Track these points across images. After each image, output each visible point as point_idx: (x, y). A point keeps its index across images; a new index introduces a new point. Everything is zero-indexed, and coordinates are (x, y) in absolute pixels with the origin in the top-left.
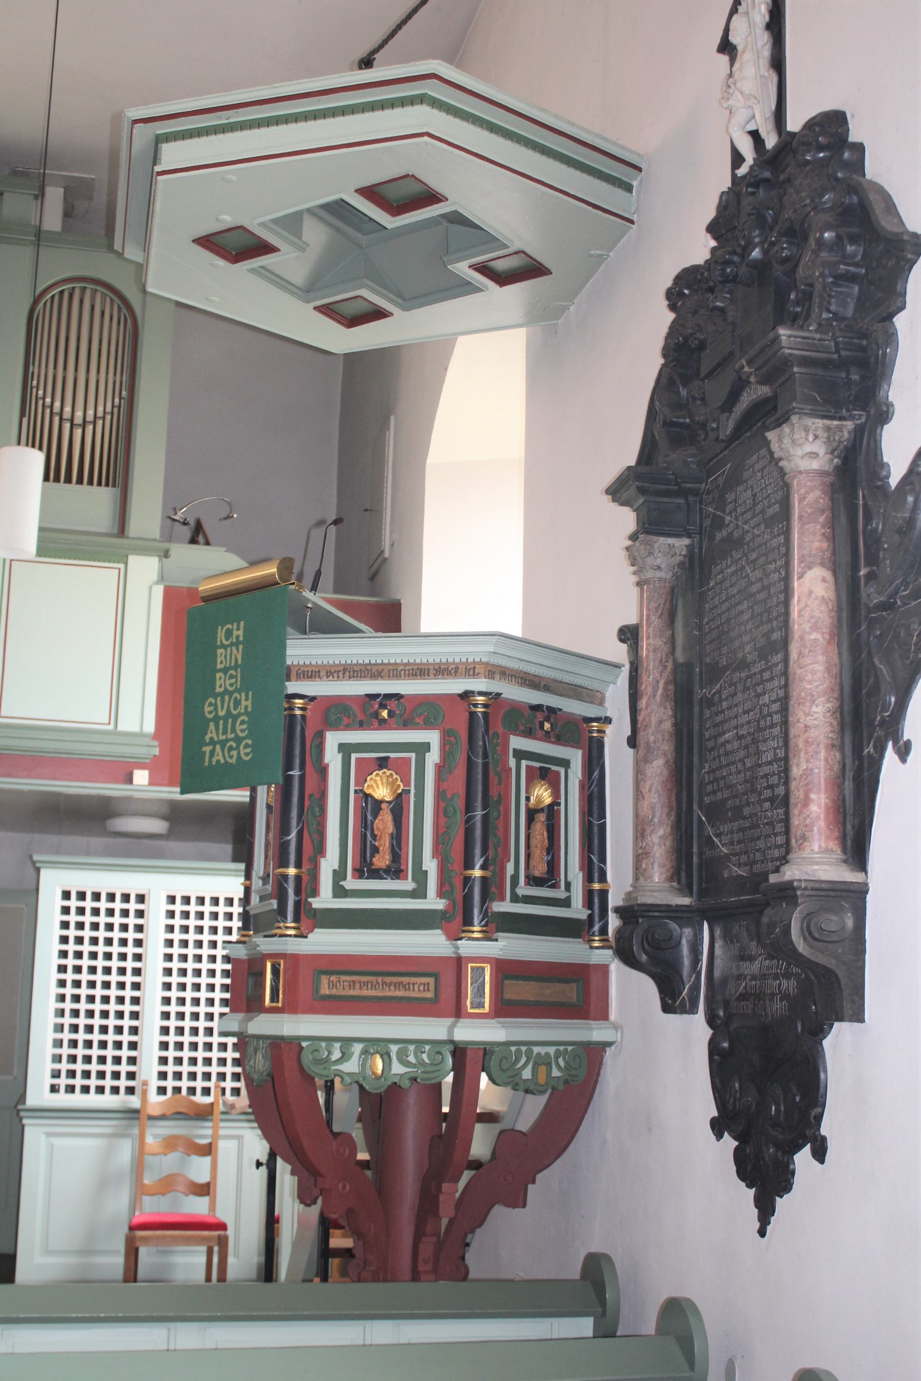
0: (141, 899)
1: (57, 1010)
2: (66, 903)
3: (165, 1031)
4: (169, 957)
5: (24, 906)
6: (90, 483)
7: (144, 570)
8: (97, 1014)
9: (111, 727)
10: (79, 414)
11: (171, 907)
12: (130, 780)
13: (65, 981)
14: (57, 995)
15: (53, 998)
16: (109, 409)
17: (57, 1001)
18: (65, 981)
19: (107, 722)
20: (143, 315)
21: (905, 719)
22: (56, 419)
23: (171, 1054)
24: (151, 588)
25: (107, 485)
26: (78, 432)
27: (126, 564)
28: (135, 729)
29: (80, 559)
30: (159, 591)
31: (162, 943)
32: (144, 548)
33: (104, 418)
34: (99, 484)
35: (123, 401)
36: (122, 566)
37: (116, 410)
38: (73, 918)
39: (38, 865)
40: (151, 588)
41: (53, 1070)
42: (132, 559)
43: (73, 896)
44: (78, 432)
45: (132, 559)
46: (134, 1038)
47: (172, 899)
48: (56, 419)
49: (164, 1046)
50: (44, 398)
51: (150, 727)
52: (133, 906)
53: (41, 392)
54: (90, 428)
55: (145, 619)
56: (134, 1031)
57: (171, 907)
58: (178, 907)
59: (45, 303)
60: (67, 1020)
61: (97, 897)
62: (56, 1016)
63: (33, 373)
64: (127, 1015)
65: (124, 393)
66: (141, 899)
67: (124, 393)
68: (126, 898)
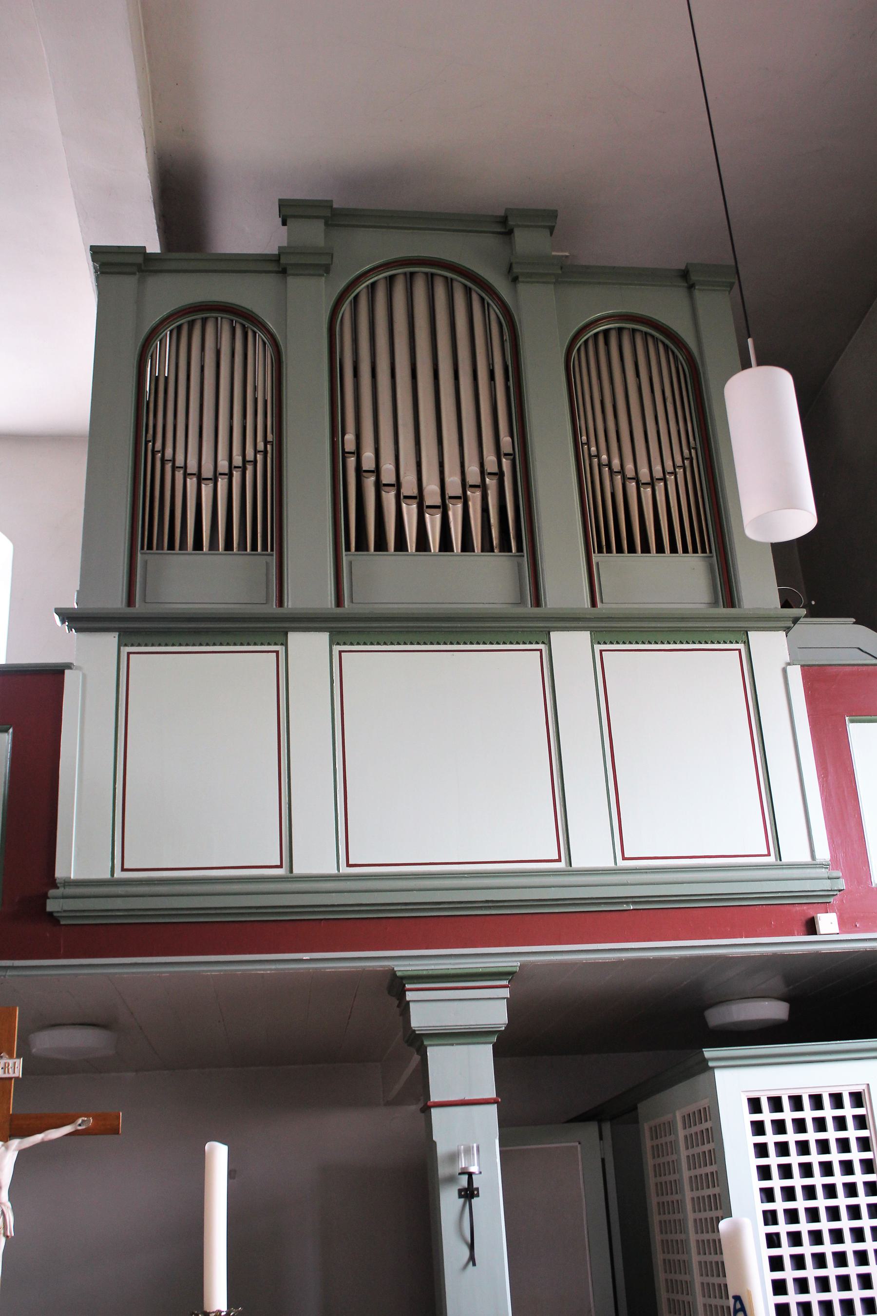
5: (577, 1144)
6: (674, 550)
10: (644, 472)
12: (811, 927)
20: (286, 347)
21: (3, 809)
24: (784, 671)
25: (695, 551)
27: (747, 643)
30: (796, 674)
32: (766, 622)
33: (675, 473)
34: (685, 551)
40: (784, 671)
44: (206, 490)
50: (598, 456)
51: (824, 853)
52: (767, 1116)
53: (593, 449)
54: (222, 483)
58: (767, 1116)
59: (579, 350)
61: (817, 1101)
65: (505, 440)
66: (858, 1099)
67: (505, 440)
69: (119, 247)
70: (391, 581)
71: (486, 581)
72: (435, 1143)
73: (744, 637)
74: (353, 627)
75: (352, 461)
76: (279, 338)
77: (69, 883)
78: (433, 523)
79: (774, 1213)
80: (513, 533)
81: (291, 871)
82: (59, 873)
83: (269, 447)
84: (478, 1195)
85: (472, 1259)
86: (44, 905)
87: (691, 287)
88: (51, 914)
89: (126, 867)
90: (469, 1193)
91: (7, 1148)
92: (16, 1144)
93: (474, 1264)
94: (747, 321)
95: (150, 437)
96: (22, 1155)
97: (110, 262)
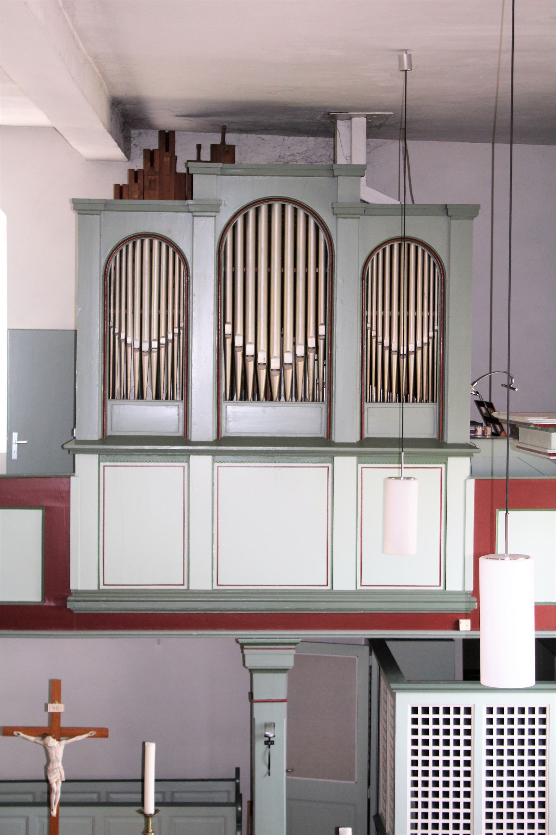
0: (468, 711)
1: (412, 803)
2: (415, 716)
3: (489, 805)
4: (490, 721)
7: (459, 467)
8: (441, 805)
9: (442, 588)
11: (490, 716)
12: (456, 627)
13: (417, 771)
14: (412, 792)
15: (409, 784)
16: (425, 340)
17: (412, 786)
18: (417, 771)
19: (438, 585)
22: (387, 353)
23: (495, 810)
26: (403, 362)
28: (459, 588)
29: (412, 463)
30: (472, 483)
31: (484, 742)
35: (436, 333)
36: (443, 466)
37: (431, 341)
38: (420, 758)
39: (394, 691)
41: (412, 803)
42: (451, 460)
43: (420, 710)
44: (403, 362)
45: (451, 460)
46: (468, 737)
47: (490, 710)
48: (387, 353)
49: (489, 815)
52: (462, 716)
55: (462, 501)
56: (467, 805)
57: (490, 768)
58: (420, 716)
60: (420, 799)
62: (412, 796)
63: (367, 316)
64: (462, 784)
66: (468, 711)
68: (457, 711)
69: (89, 200)
70: (245, 418)
71: (303, 418)
72: (176, 157)
73: (445, 461)
74: (369, 447)
75: (229, 342)
76: (188, 258)
77: (78, 592)
78: (276, 380)
79: (416, 803)
80: (322, 392)
81: (189, 586)
82: (73, 587)
83: (181, 331)
84: (273, 744)
85: (269, 774)
86: (66, 605)
87: (451, 219)
88: (69, 609)
89: (105, 583)
90: (269, 743)
91: (60, 745)
92: (64, 742)
93: (269, 775)
94: (492, 491)
95: (112, 324)
96: (66, 747)
97: (83, 208)
